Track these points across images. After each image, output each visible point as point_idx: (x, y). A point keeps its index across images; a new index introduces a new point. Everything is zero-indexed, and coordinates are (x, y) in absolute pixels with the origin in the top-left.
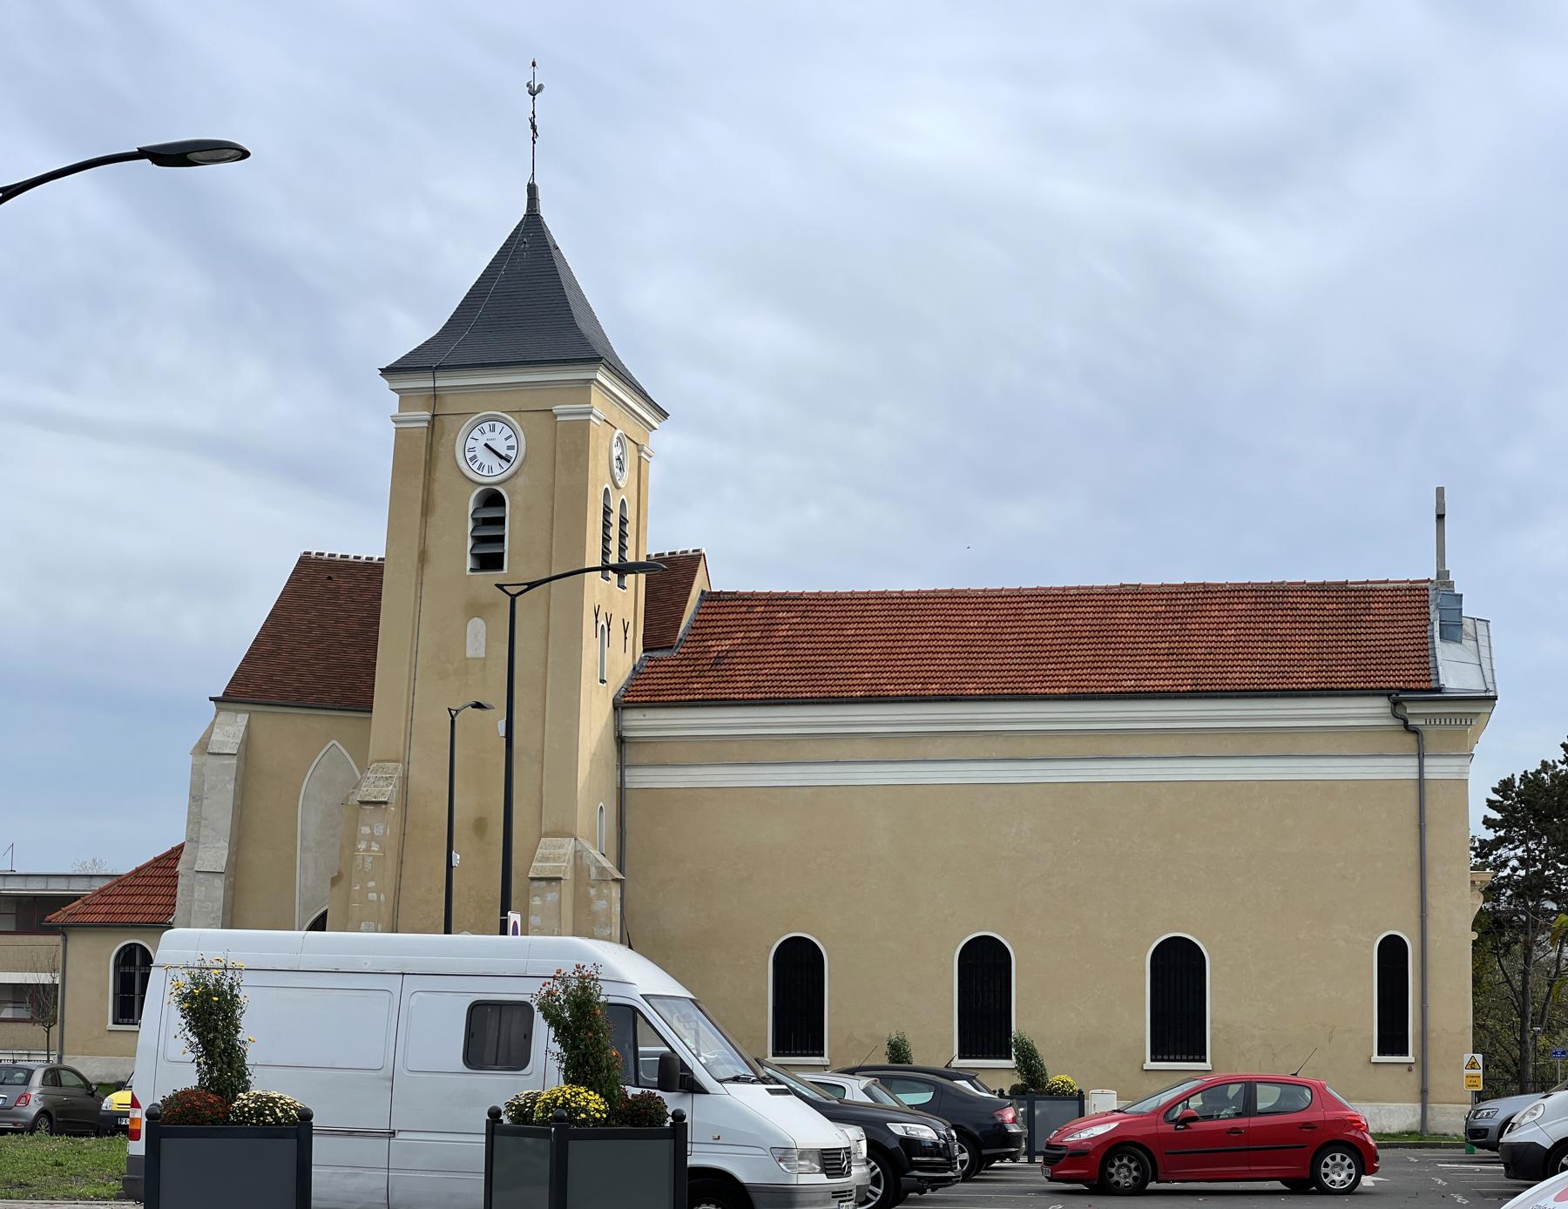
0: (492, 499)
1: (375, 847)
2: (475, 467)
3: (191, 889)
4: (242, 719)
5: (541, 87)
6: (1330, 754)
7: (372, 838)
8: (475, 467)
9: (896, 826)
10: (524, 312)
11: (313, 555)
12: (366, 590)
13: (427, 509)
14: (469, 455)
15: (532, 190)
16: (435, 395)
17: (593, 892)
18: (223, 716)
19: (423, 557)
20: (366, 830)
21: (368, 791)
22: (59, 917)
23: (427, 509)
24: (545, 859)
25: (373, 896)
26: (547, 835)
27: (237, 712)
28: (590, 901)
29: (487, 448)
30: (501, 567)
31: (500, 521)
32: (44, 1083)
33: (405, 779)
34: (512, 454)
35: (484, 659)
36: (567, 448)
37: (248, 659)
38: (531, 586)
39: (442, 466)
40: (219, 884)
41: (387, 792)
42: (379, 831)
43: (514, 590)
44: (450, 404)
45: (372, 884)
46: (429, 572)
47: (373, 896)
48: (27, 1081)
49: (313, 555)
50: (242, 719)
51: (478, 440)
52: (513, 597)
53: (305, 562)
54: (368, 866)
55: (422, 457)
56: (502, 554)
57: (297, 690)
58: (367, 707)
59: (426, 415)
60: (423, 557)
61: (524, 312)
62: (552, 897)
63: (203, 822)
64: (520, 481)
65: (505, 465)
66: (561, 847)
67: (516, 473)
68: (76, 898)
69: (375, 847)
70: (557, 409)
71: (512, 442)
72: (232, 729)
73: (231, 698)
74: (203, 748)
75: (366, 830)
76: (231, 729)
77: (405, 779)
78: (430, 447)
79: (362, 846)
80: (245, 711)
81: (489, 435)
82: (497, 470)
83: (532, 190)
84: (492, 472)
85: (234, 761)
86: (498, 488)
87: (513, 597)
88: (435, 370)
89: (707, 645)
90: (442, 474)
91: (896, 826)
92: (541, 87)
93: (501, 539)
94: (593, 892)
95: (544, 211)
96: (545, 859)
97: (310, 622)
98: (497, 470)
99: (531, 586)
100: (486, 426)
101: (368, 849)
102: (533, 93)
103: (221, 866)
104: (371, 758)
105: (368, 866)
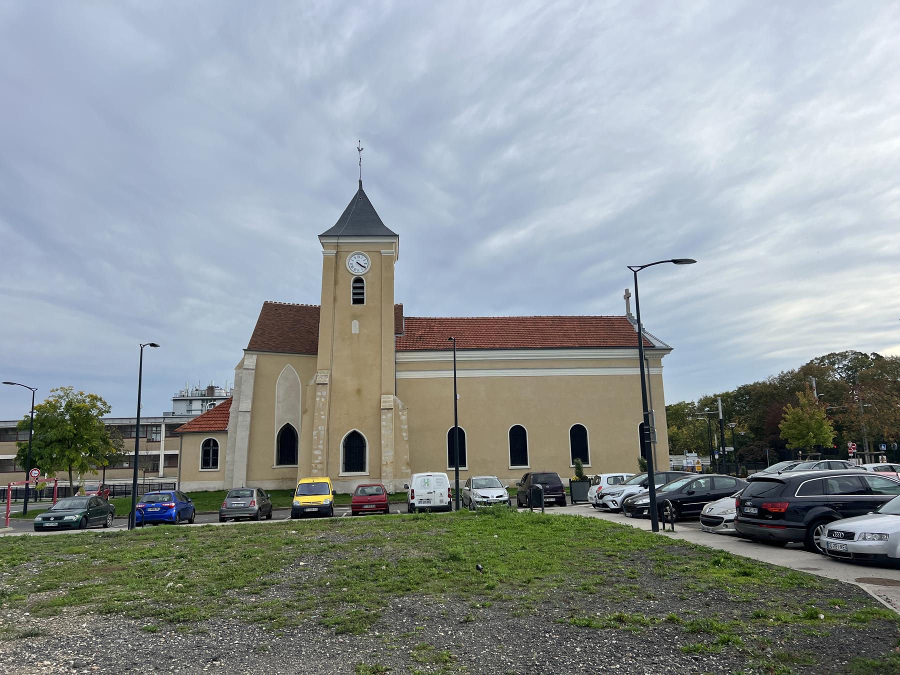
0: (359, 280)
3: (237, 417)
4: (255, 357)
6: (618, 368)
7: (321, 396)
9: (498, 389)
13: (336, 283)
15: (360, 182)
16: (338, 245)
19: (335, 299)
20: (319, 394)
22: (179, 430)
23: (336, 283)
29: (357, 263)
32: (258, 495)
33: (331, 375)
38: (642, 267)
39: (341, 267)
41: (327, 381)
42: (324, 393)
43: (635, 269)
44: (344, 248)
48: (252, 496)
50: (255, 357)
52: (635, 272)
53: (266, 304)
55: (333, 266)
58: (312, 349)
60: (335, 299)
62: (389, 415)
64: (369, 275)
68: (181, 425)
72: (251, 361)
74: (240, 366)
75: (319, 394)
77: (331, 375)
78: (336, 262)
79: (318, 399)
83: (360, 182)
84: (359, 272)
87: (635, 272)
89: (416, 335)
90: (341, 272)
91: (498, 389)
99: (642, 267)
103: (249, 409)
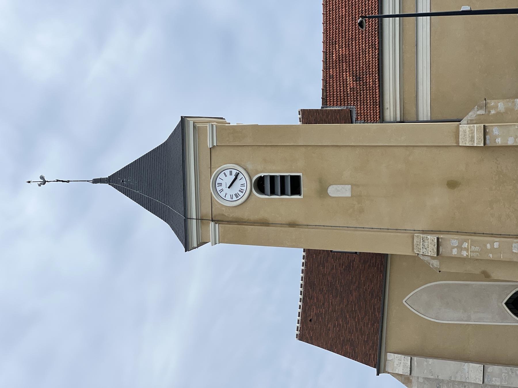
0: (260, 185)
1: (465, 245)
2: (241, 194)
4: (390, 356)
5: (42, 177)
7: (460, 248)
8: (241, 194)
10: (158, 181)
11: (298, 333)
12: (317, 299)
13: (265, 223)
14: (235, 198)
15: (96, 181)
16: (201, 220)
17: (493, 112)
18: (389, 369)
19: (292, 225)
21: (431, 250)
23: (265, 223)
24: (472, 139)
25: (496, 245)
26: (458, 142)
27: (386, 360)
28: (498, 113)
29: (229, 188)
30: (298, 177)
31: (272, 178)
33: (424, 232)
34: (234, 172)
35: (353, 185)
36: (235, 139)
37: (354, 357)
40: (490, 369)
41: (432, 238)
44: (206, 210)
45: (488, 246)
46: (301, 220)
47: (496, 245)
49: (298, 333)
50: (390, 356)
51: (227, 193)
53: (301, 337)
54: (477, 249)
55: (236, 227)
56: (292, 177)
57: (373, 325)
59: (212, 224)
60: (292, 225)
61: (158, 181)
63: (453, 379)
64: (250, 167)
65: (240, 175)
66: (465, 132)
67: (245, 169)
69: (465, 245)
70: (210, 145)
71: (227, 172)
72: (397, 362)
73: (377, 362)
75: (455, 252)
76: (396, 362)
77: (424, 232)
78: (230, 222)
79: (465, 254)
80: (386, 355)
81: (223, 187)
82: (243, 181)
84: (245, 184)
85: (415, 359)
86: (254, 179)
88: (186, 219)
89: (353, 87)
90: (246, 214)
92: (42, 177)
93: (283, 178)
94: (493, 112)
95: (106, 175)
96: (472, 139)
97: (334, 326)
98: (243, 181)
100: (219, 189)
101: (467, 250)
102: (44, 182)
103: (480, 367)
104: (409, 253)
105: (477, 249)
